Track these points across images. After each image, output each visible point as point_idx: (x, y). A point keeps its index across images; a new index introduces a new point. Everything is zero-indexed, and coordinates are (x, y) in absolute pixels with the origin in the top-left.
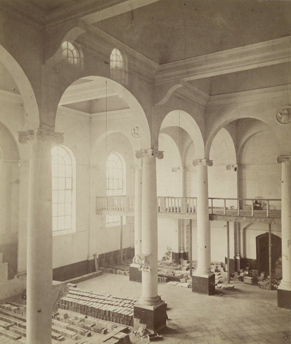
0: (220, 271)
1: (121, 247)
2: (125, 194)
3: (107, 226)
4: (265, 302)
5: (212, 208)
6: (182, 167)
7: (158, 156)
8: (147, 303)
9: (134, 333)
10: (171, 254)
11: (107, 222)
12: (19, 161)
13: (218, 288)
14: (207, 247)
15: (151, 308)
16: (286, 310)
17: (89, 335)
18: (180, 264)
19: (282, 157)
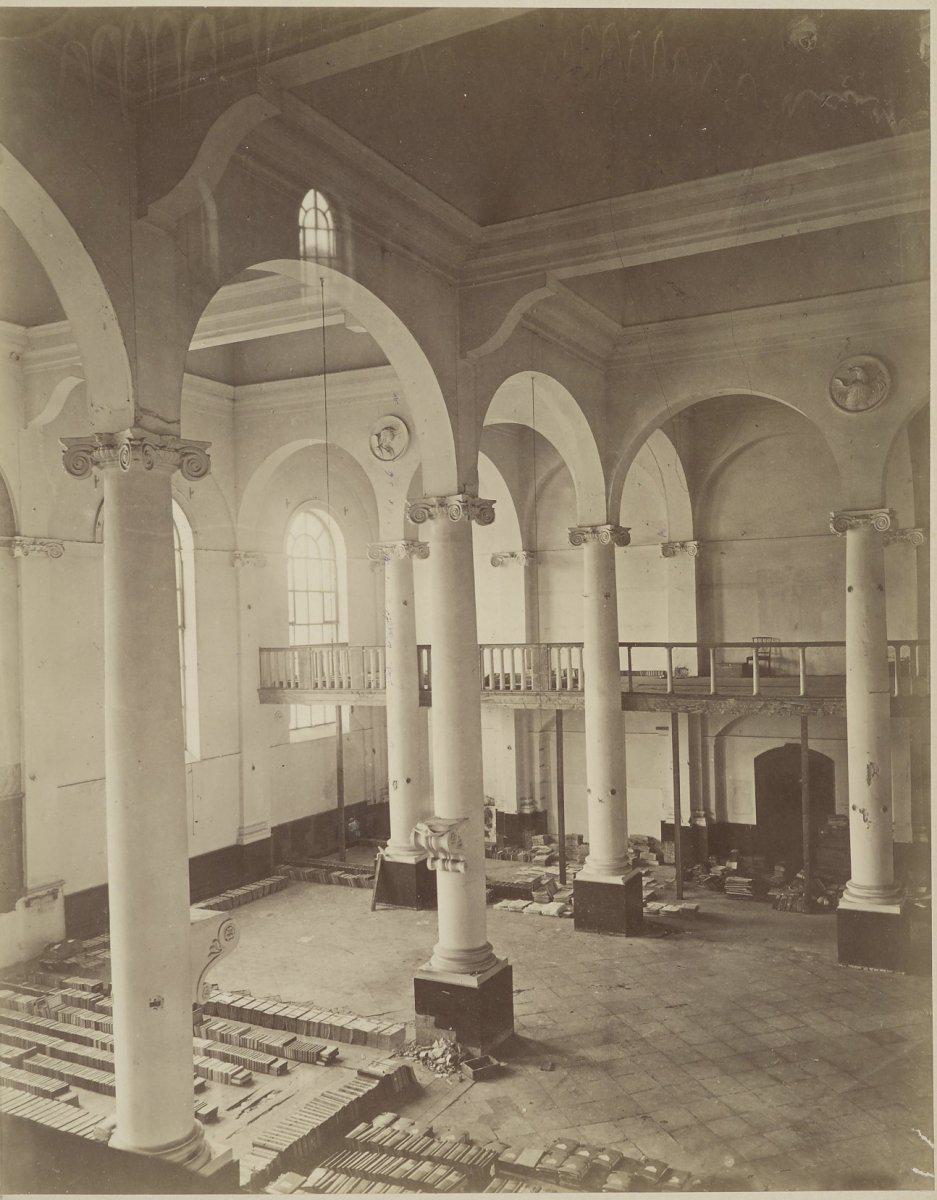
0: (648, 865)
1: (341, 800)
2: (344, 638)
3: (294, 737)
4: (796, 949)
5: (630, 673)
6: (524, 553)
7: (478, 516)
8: (454, 965)
9: (419, 1058)
10: (494, 817)
11: (292, 726)
12: (16, 538)
13: (650, 913)
14: (617, 791)
15: (472, 982)
16: (865, 969)
17: (283, 1071)
18: (522, 846)
19: (850, 513)
